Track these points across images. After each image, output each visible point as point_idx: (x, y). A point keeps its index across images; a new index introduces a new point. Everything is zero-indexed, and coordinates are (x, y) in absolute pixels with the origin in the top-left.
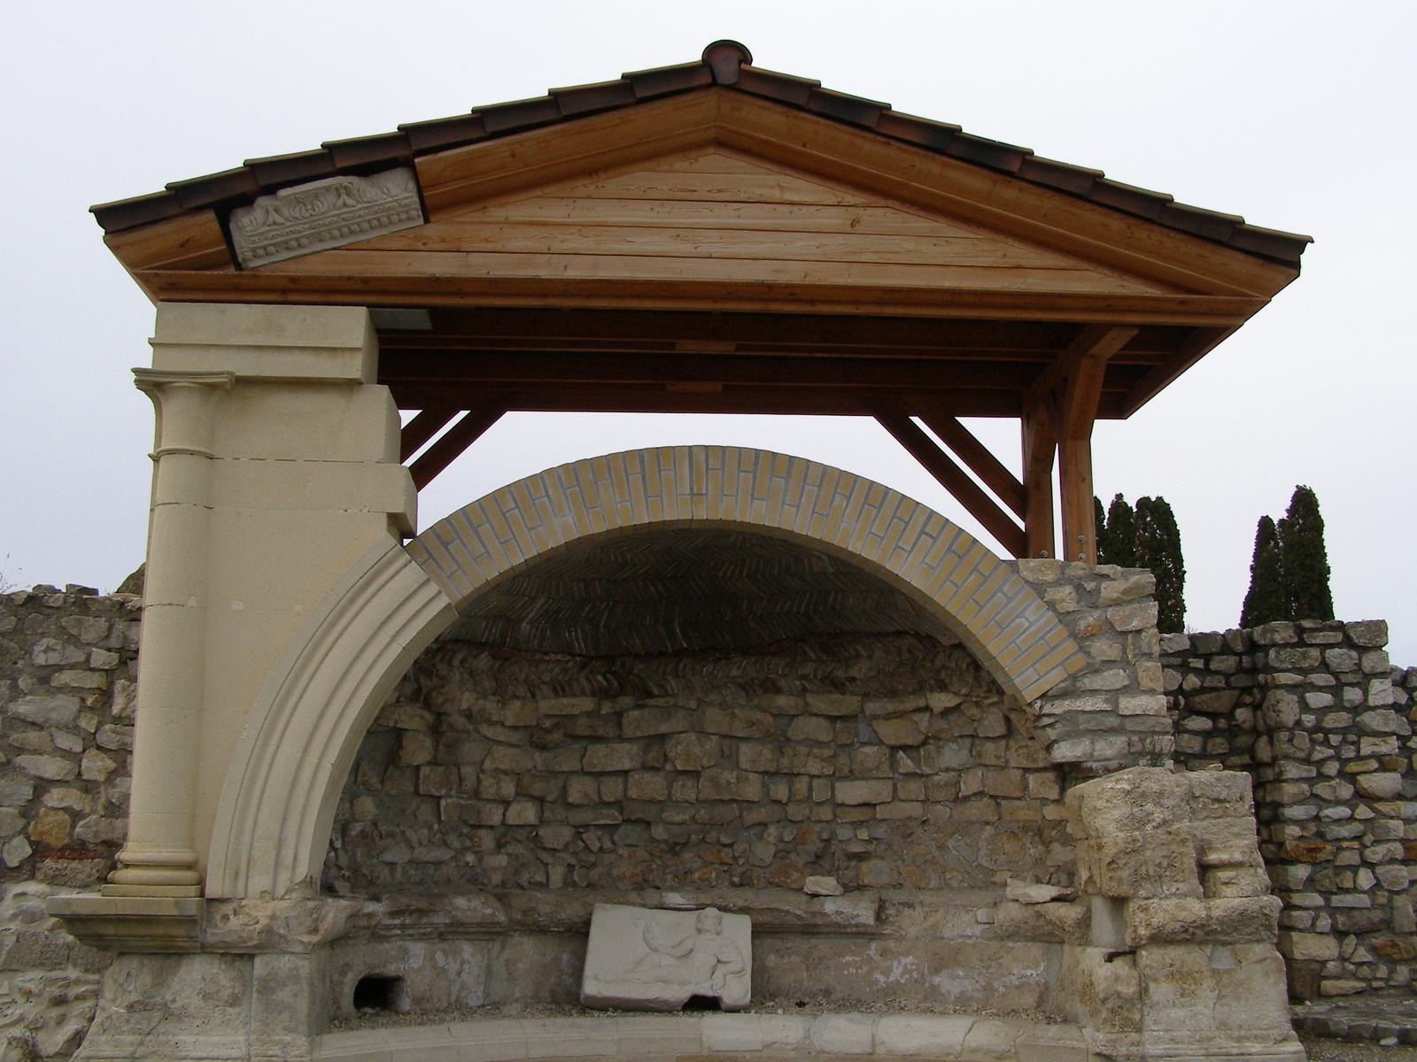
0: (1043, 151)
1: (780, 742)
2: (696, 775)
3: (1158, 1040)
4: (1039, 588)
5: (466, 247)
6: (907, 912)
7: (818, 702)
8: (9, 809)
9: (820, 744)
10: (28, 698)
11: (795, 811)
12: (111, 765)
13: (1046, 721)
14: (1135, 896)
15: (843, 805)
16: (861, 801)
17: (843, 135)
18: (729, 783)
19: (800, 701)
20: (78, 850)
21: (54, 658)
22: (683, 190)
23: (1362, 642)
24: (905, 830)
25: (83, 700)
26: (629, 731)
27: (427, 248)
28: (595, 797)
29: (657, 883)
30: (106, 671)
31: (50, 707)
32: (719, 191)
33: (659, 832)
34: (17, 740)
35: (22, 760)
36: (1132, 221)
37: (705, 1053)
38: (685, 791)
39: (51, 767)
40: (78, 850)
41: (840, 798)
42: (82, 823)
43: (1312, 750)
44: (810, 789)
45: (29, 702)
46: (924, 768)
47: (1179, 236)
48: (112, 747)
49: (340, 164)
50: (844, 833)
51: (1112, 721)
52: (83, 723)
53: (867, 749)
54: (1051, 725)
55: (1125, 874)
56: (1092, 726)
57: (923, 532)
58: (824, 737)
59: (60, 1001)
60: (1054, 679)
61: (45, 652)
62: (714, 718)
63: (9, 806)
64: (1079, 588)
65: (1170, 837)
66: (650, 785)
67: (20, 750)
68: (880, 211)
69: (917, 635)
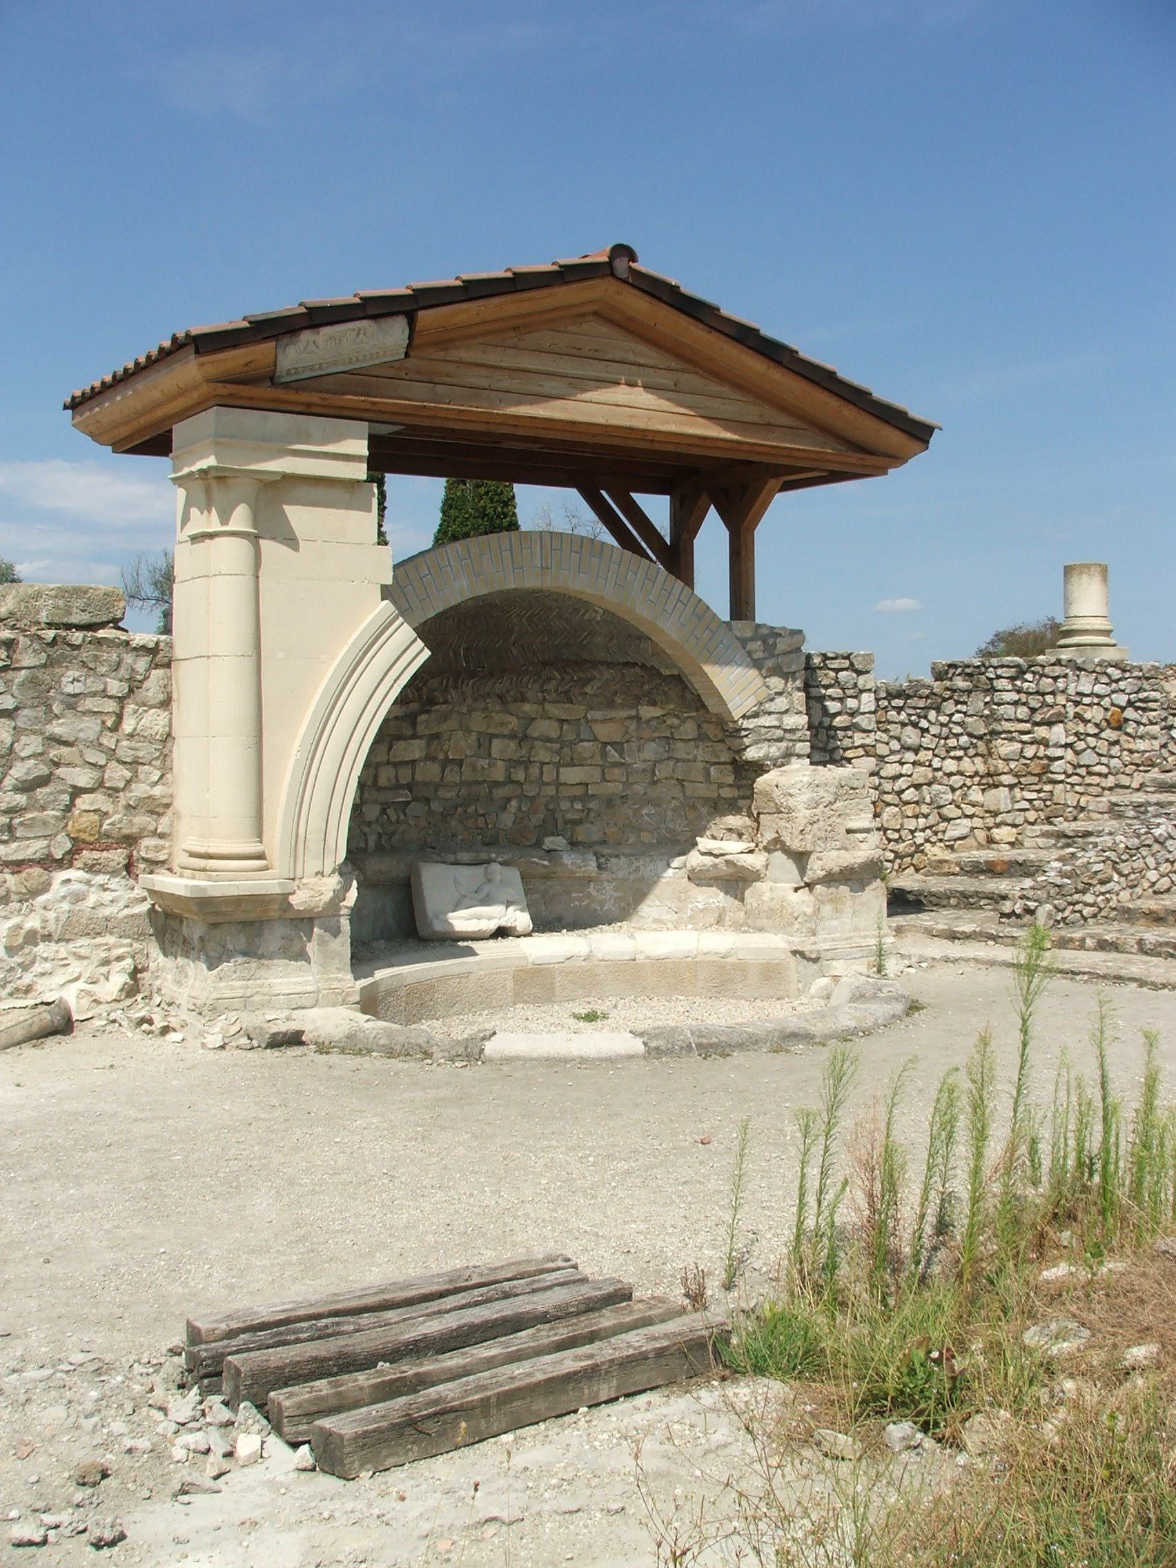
0: (804, 354)
1: (522, 738)
2: (460, 763)
3: (825, 940)
4: (744, 642)
5: (436, 380)
6: (613, 860)
7: (554, 710)
8: (54, 813)
9: (549, 740)
10: (61, 721)
11: (531, 791)
12: (128, 775)
13: (743, 733)
14: (814, 851)
15: (566, 784)
16: (578, 781)
17: (683, 321)
18: (483, 768)
19: (540, 708)
20: (104, 841)
21: (77, 688)
22: (572, 348)
23: (859, 667)
24: (609, 802)
25: (103, 722)
26: (421, 729)
27: (407, 378)
28: (394, 781)
29: (434, 845)
30: (119, 697)
31: (79, 728)
32: (596, 351)
33: (436, 806)
34: (55, 756)
35: (61, 772)
36: (842, 402)
37: (530, 966)
38: (452, 776)
39: (83, 778)
40: (104, 841)
41: (562, 779)
42: (108, 822)
43: (828, 742)
44: (542, 773)
45: (62, 724)
46: (627, 758)
47: (868, 416)
48: (128, 760)
49: (369, 313)
50: (565, 805)
51: (779, 733)
52: (105, 741)
53: (586, 744)
54: (746, 736)
55: (809, 837)
56: (768, 736)
57: (679, 600)
58: (554, 735)
59: (106, 962)
60: (749, 705)
61: (72, 683)
62: (477, 722)
63: (53, 809)
64: (764, 642)
65: (832, 813)
66: (430, 772)
67: (57, 765)
68: (692, 376)
69: (643, 666)
